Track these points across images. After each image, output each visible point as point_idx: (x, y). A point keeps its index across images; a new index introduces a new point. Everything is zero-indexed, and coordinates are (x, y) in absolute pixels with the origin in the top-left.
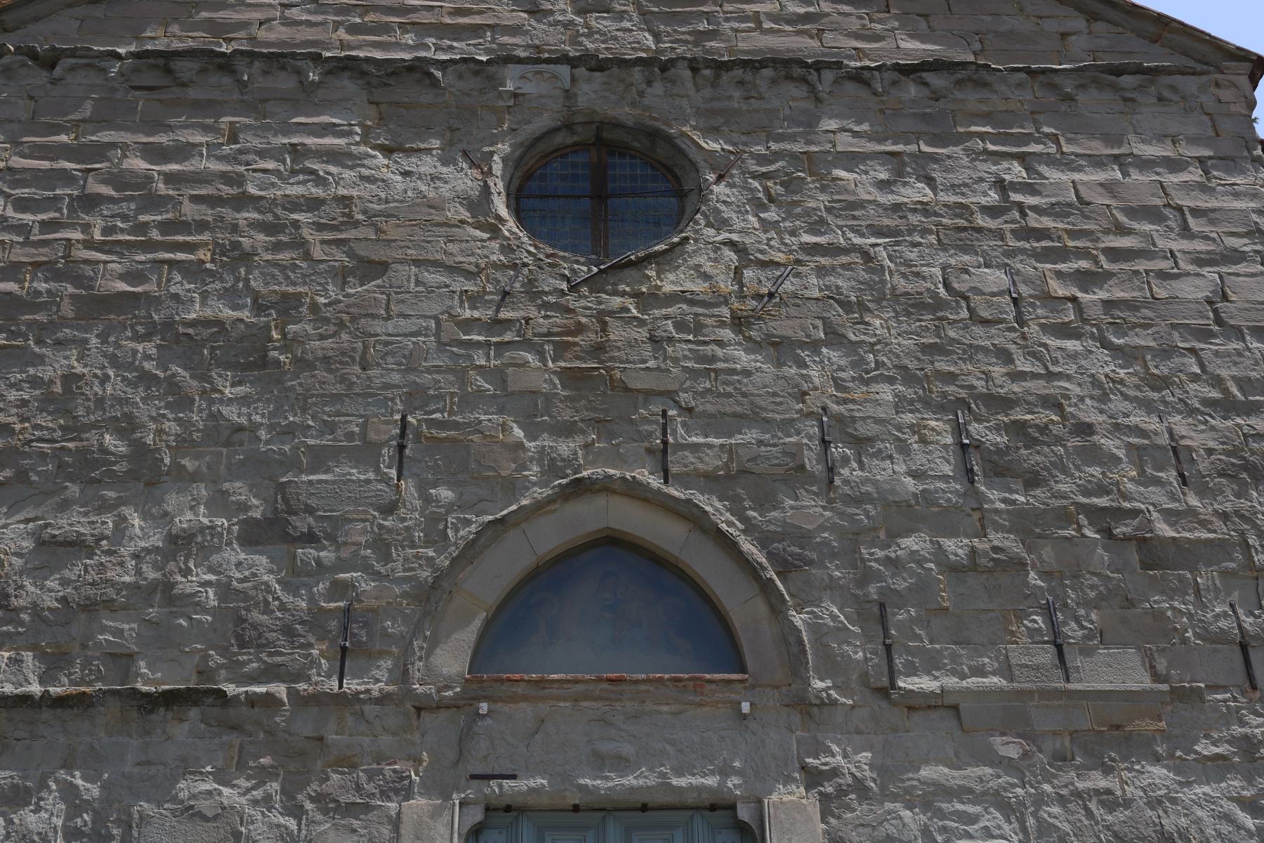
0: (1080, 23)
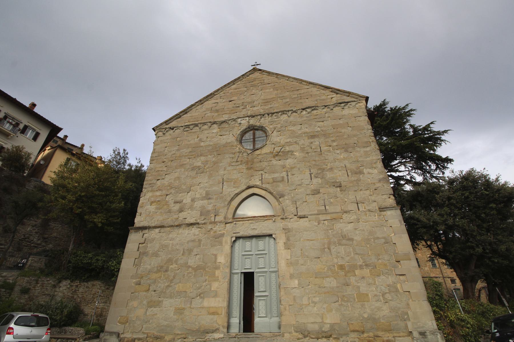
0: (335, 95)
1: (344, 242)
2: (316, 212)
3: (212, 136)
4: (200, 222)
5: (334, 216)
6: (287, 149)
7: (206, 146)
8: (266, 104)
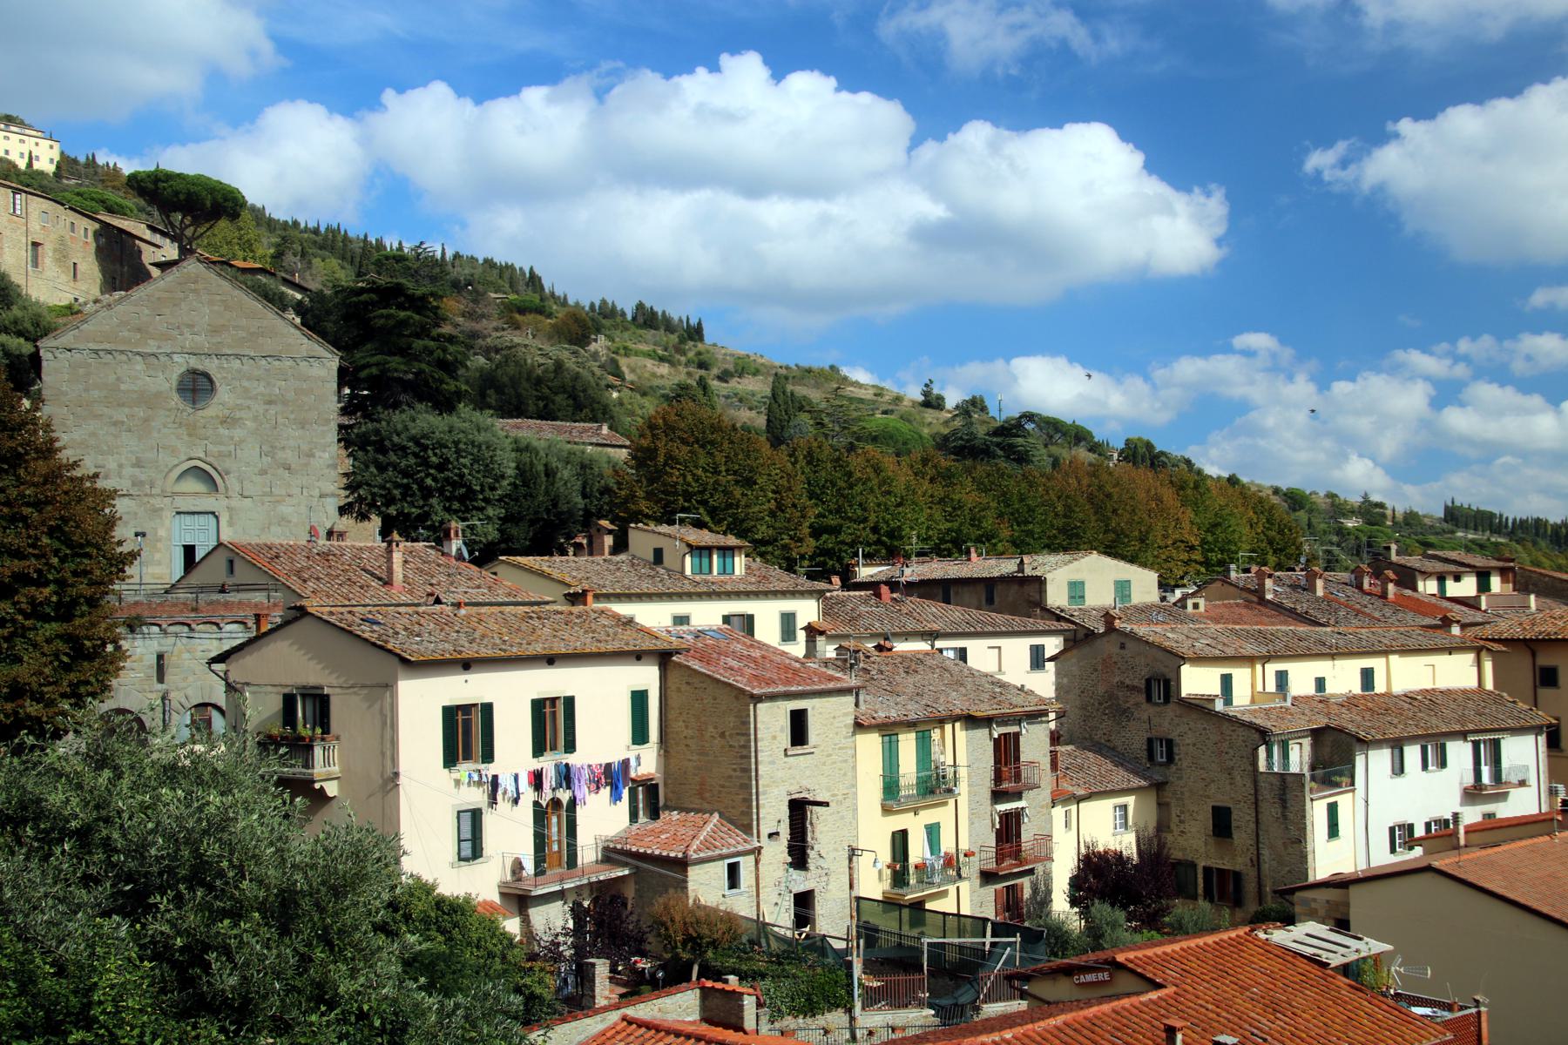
6: (238, 415)
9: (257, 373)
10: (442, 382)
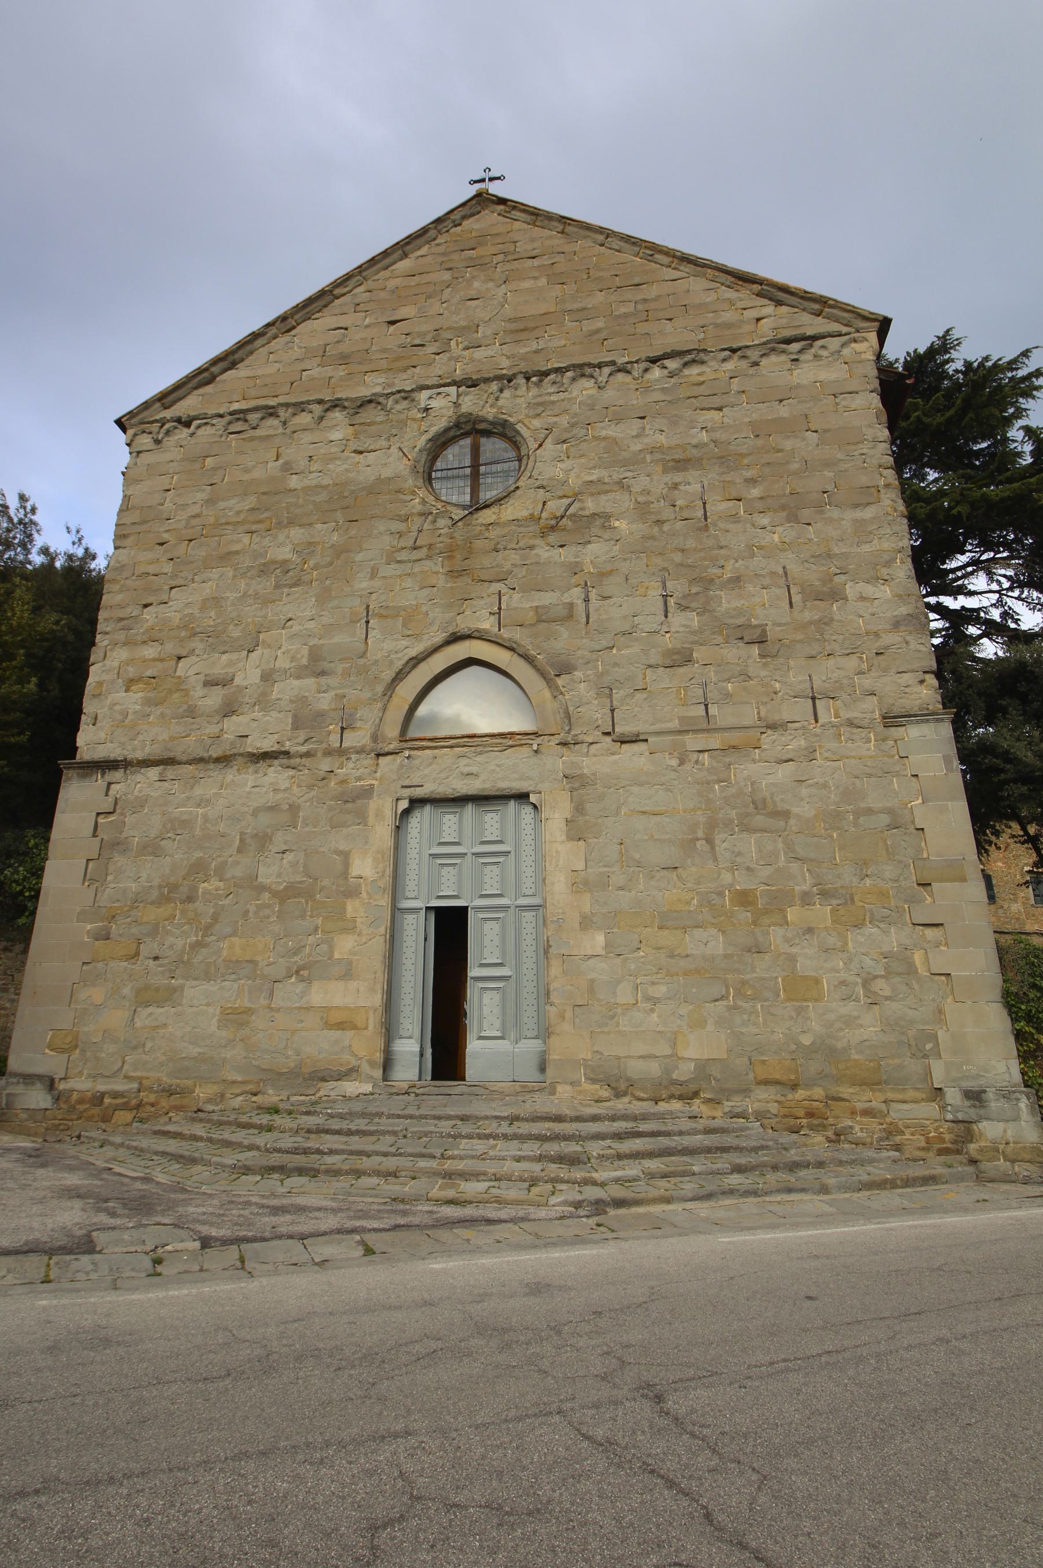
0: (770, 309)
1: (759, 820)
2: (675, 724)
3: (326, 454)
4: (293, 750)
5: (734, 737)
7: (306, 490)
8: (523, 336)
9: (636, 400)
10: (943, 415)
